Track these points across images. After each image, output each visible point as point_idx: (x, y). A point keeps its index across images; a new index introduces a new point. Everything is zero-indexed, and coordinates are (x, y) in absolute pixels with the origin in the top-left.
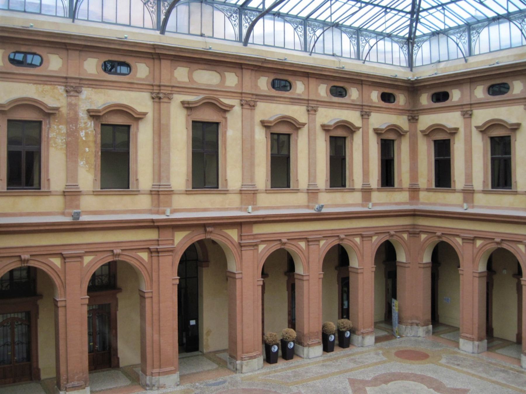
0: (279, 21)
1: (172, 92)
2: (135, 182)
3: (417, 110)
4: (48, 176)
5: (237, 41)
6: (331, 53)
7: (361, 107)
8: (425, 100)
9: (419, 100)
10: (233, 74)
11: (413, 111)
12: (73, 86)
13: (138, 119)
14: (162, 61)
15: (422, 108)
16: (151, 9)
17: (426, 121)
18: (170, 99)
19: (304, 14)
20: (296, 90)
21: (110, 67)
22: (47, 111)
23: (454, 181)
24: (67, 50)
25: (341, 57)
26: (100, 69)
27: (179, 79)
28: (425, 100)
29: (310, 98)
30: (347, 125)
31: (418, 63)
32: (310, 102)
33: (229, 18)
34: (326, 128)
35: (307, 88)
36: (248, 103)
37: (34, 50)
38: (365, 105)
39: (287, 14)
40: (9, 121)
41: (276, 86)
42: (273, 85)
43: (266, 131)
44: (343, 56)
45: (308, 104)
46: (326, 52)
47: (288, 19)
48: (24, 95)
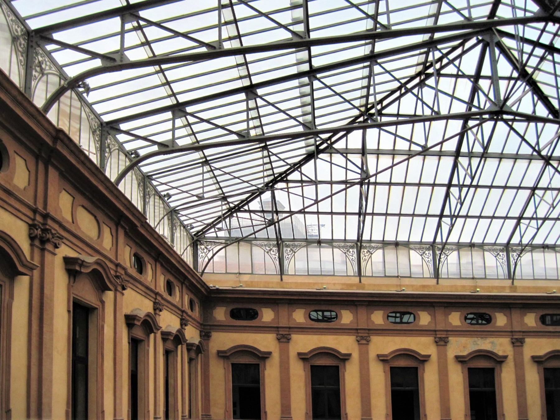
0: (548, 252)
1: (448, 336)
2: (345, 416)
3: (210, 326)
4: (345, 410)
5: (506, 279)
6: (472, 277)
7: (434, 333)
8: (220, 314)
9: (212, 314)
10: (502, 314)
11: (204, 325)
12: (363, 335)
13: (501, 363)
14: (436, 308)
15: (215, 323)
16: (274, 256)
17: (224, 340)
18: (446, 343)
19: (503, 240)
20: (419, 321)
21: (235, 314)
22: (341, 357)
23: (266, 412)
24: (356, 305)
25: (485, 278)
26: (540, 323)
27: (298, 321)
28: (220, 314)
29: (513, 330)
30: (415, 355)
31: (443, 271)
32: (437, 333)
33: (268, 252)
34: (462, 360)
35: (434, 317)
36: (283, 336)
37: (410, 311)
38: (515, 332)
39: (555, 244)
40: (312, 366)
41: (547, 323)
42: (543, 320)
43: (304, 366)
44: (487, 277)
45: (436, 334)
46: (462, 276)
47: (486, 247)
48: (322, 345)
